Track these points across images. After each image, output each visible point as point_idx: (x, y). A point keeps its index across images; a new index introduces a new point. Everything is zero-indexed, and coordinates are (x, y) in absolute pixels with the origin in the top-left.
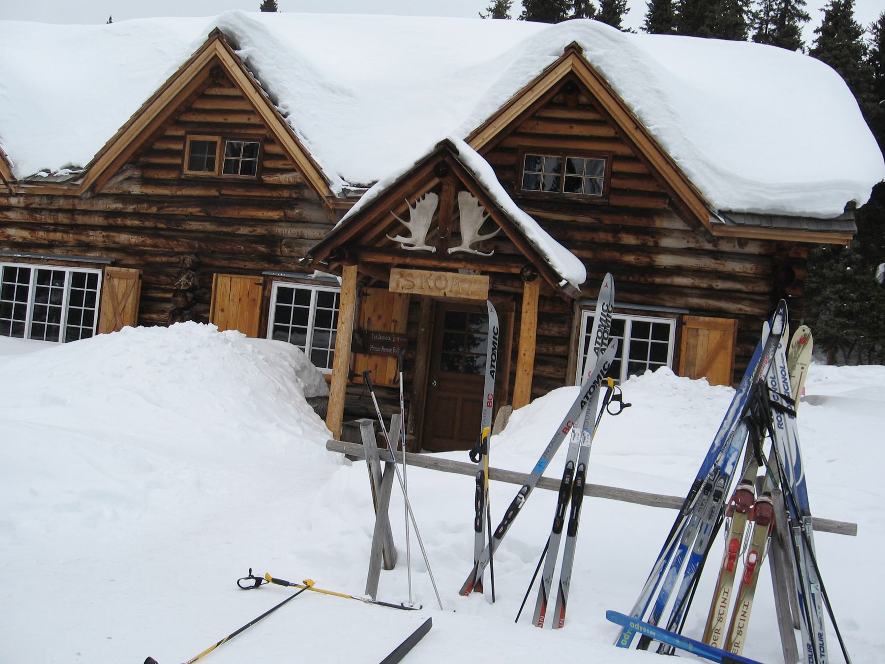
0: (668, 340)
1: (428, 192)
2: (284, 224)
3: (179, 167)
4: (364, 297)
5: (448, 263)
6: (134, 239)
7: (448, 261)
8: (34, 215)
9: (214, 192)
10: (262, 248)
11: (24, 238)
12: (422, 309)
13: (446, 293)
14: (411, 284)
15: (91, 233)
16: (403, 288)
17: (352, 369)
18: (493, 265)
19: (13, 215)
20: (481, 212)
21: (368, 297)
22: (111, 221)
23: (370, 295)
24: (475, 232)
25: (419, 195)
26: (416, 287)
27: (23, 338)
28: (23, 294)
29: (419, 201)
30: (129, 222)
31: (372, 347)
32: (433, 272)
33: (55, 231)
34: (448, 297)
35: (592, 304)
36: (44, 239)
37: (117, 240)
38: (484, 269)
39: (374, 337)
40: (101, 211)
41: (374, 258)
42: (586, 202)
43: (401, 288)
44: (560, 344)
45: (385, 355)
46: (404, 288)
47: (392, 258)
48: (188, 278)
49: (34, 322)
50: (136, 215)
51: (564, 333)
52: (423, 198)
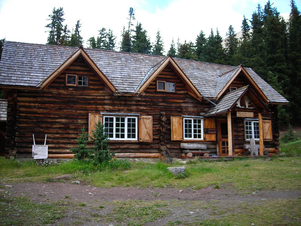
0: (132, 138)
2: (183, 104)
3: (156, 88)
6: (145, 108)
9: (165, 95)
10: (179, 110)
11: (110, 109)
15: (132, 107)
17: (204, 137)
19: (106, 102)
22: (138, 103)
27: (113, 138)
28: (112, 125)
30: (143, 103)
31: (209, 132)
33: (121, 106)
34: (238, 117)
35: (31, 146)
36: (117, 109)
37: (140, 108)
39: (209, 129)
40: (135, 101)
42: (60, 136)
44: (242, 128)
45: (211, 134)
48: (165, 118)
49: (124, 133)
50: (144, 101)
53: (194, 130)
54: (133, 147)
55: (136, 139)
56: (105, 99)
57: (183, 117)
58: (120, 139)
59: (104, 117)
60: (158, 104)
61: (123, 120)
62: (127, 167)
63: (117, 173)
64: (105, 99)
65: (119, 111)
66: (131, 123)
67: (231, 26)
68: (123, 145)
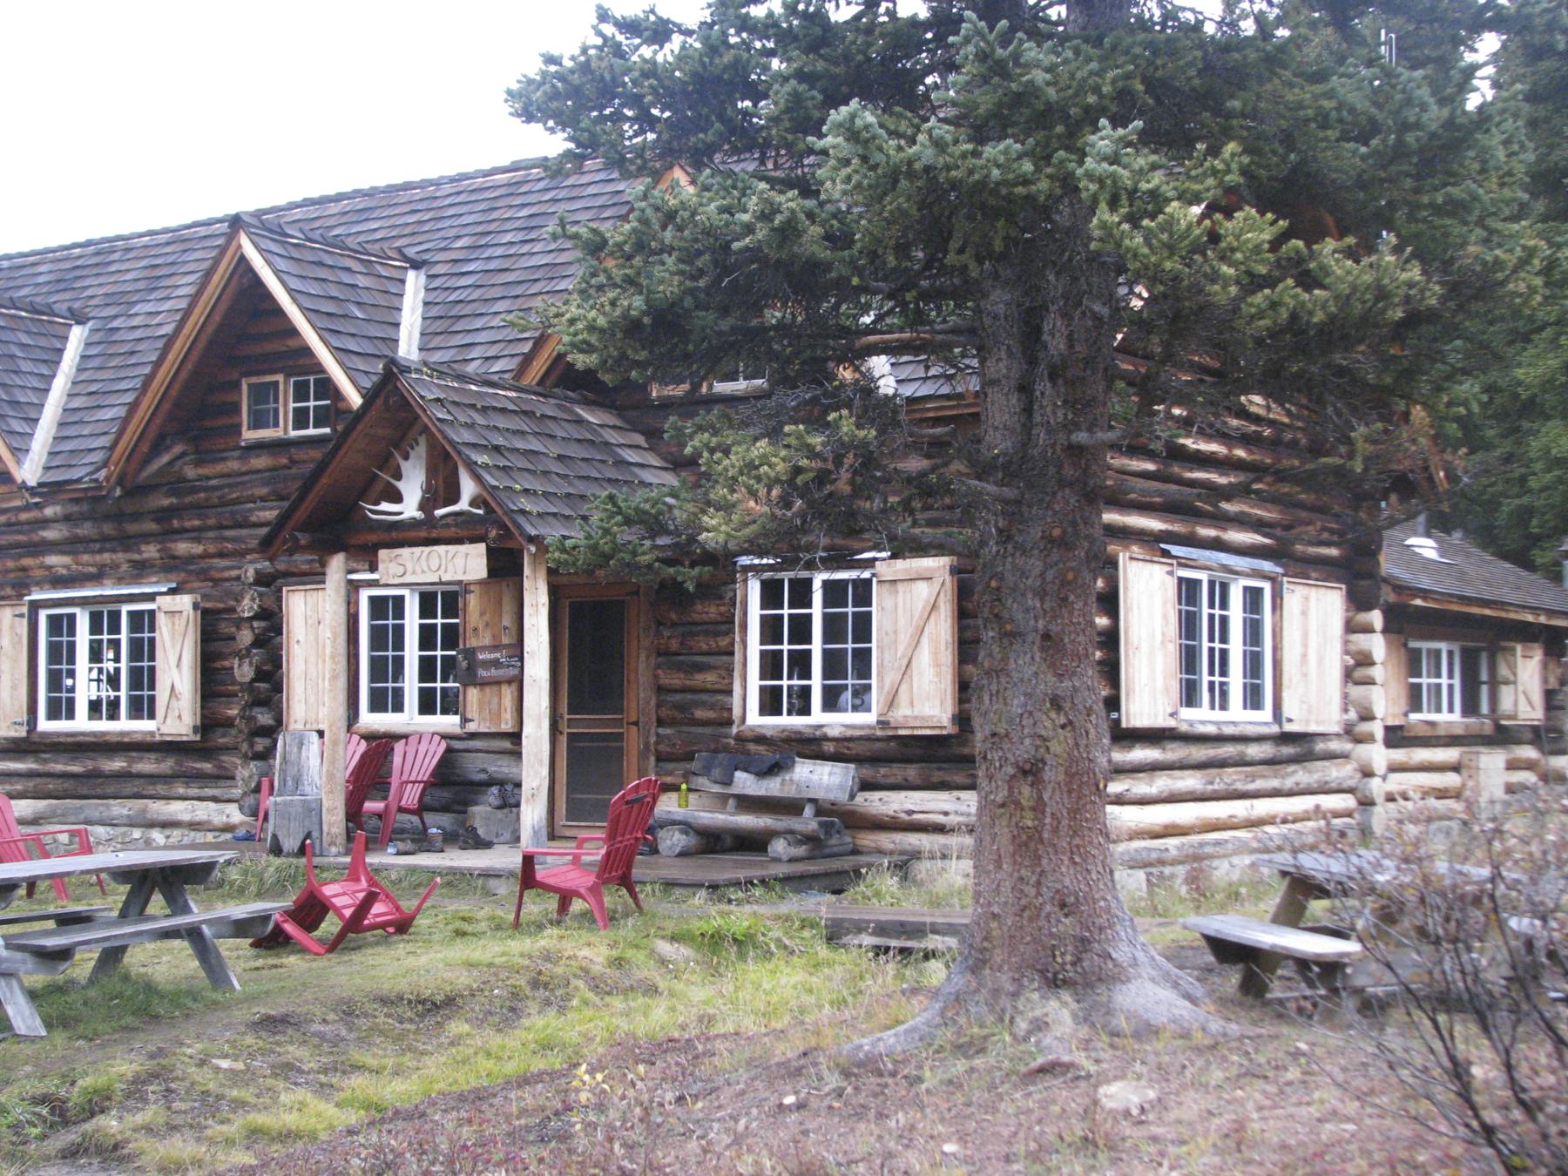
19: (50, 534)
48: (253, 600)
53: (806, 674)
54: (1253, 751)
55: (868, 718)
56: (45, 523)
57: (32, 603)
58: (787, 721)
59: (43, 615)
60: (253, 519)
61: (801, 594)
62: (522, 955)
63: (752, 976)
64: (45, 523)
65: (96, 578)
66: (786, 611)
67: (599, 7)
68: (1131, 748)
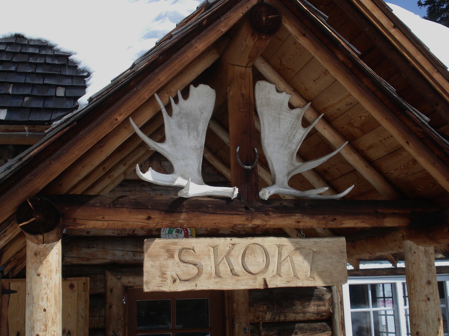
1: (196, 83)
4: (6, 296)
5: (266, 218)
7: (267, 214)
8: (293, 307)
12: (111, 307)
13: (268, 280)
14: (194, 271)
16: (174, 281)
18: (353, 214)
20: (298, 118)
21: (12, 295)
23: (15, 292)
24: (292, 158)
25: (177, 89)
26: (203, 276)
29: (176, 100)
32: (236, 240)
38: (333, 225)
41: (103, 219)
43: (170, 280)
46: (178, 281)
47: (145, 217)
51: (323, 314)
52: (186, 94)
